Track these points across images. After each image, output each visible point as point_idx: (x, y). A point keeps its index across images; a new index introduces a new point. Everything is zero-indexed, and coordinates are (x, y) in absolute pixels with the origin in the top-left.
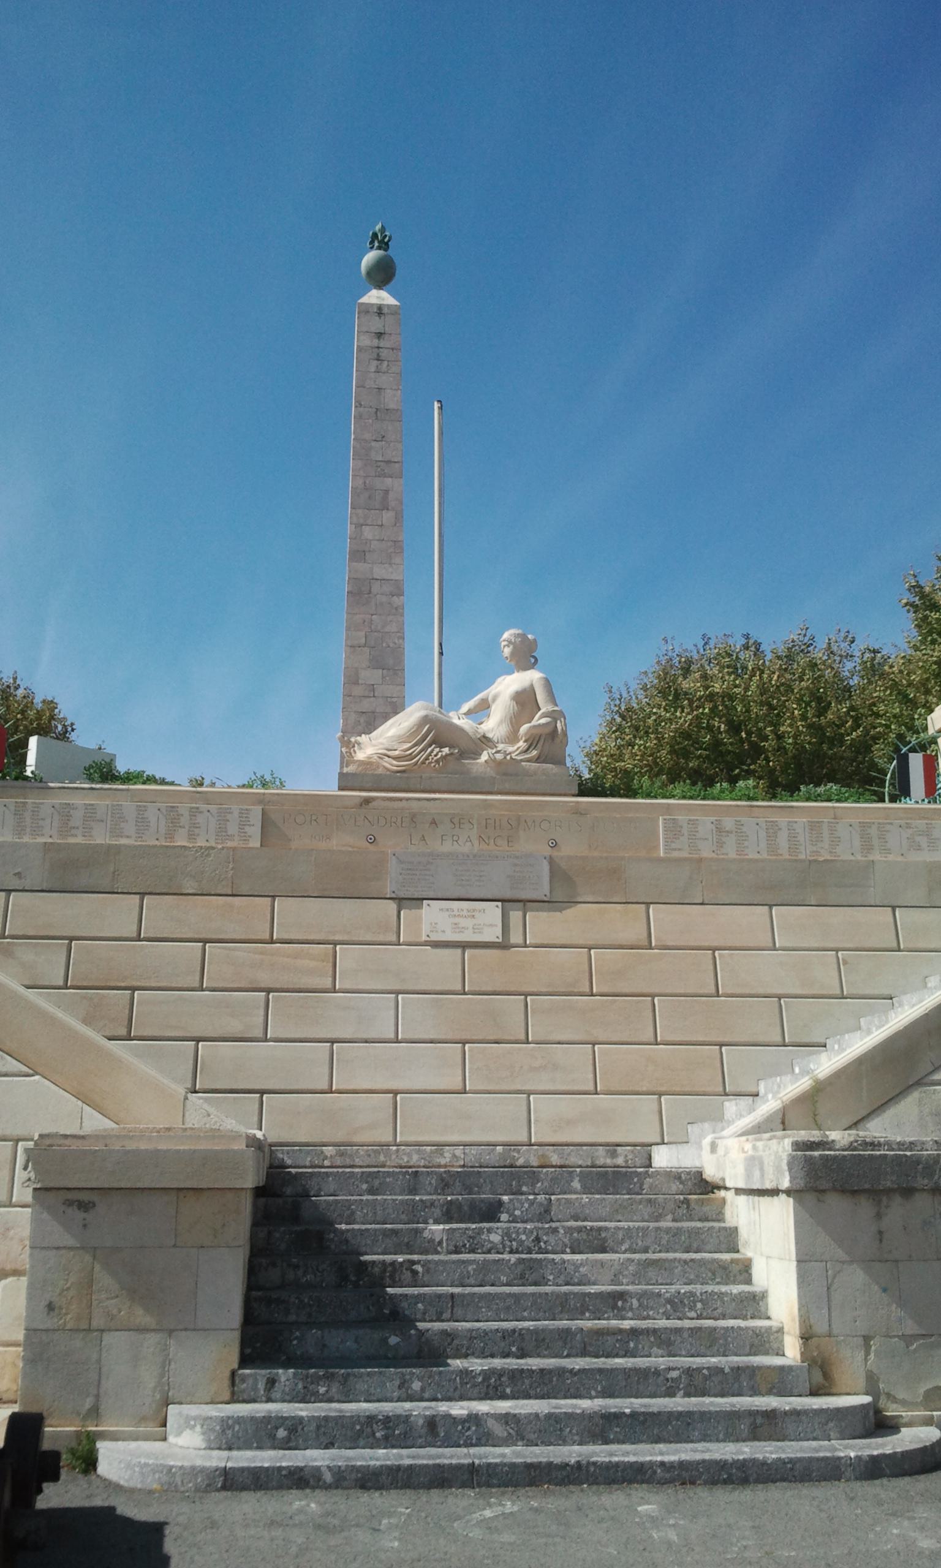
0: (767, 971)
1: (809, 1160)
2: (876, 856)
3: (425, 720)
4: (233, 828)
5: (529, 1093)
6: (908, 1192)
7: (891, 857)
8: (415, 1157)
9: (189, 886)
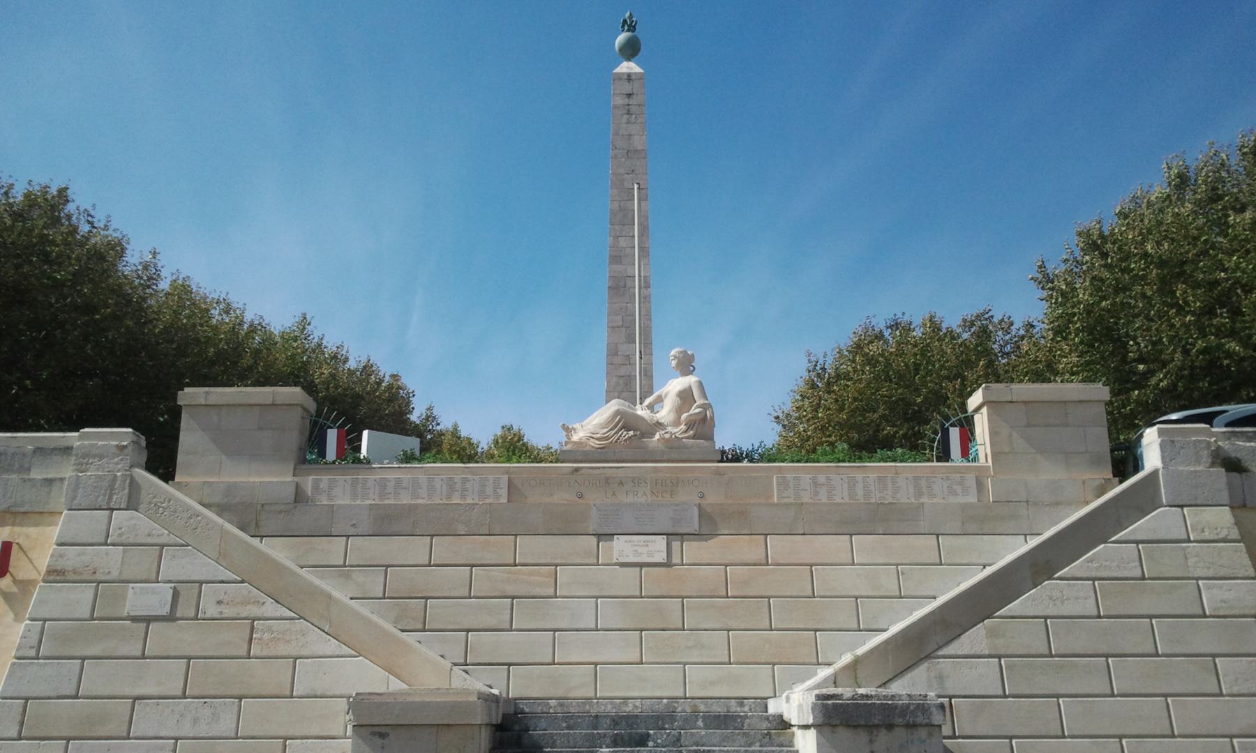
0: (849, 580)
1: (825, 706)
2: (925, 500)
3: (617, 413)
4: (489, 491)
5: (685, 664)
6: (890, 727)
7: (935, 500)
8: (609, 707)
9: (461, 529)
